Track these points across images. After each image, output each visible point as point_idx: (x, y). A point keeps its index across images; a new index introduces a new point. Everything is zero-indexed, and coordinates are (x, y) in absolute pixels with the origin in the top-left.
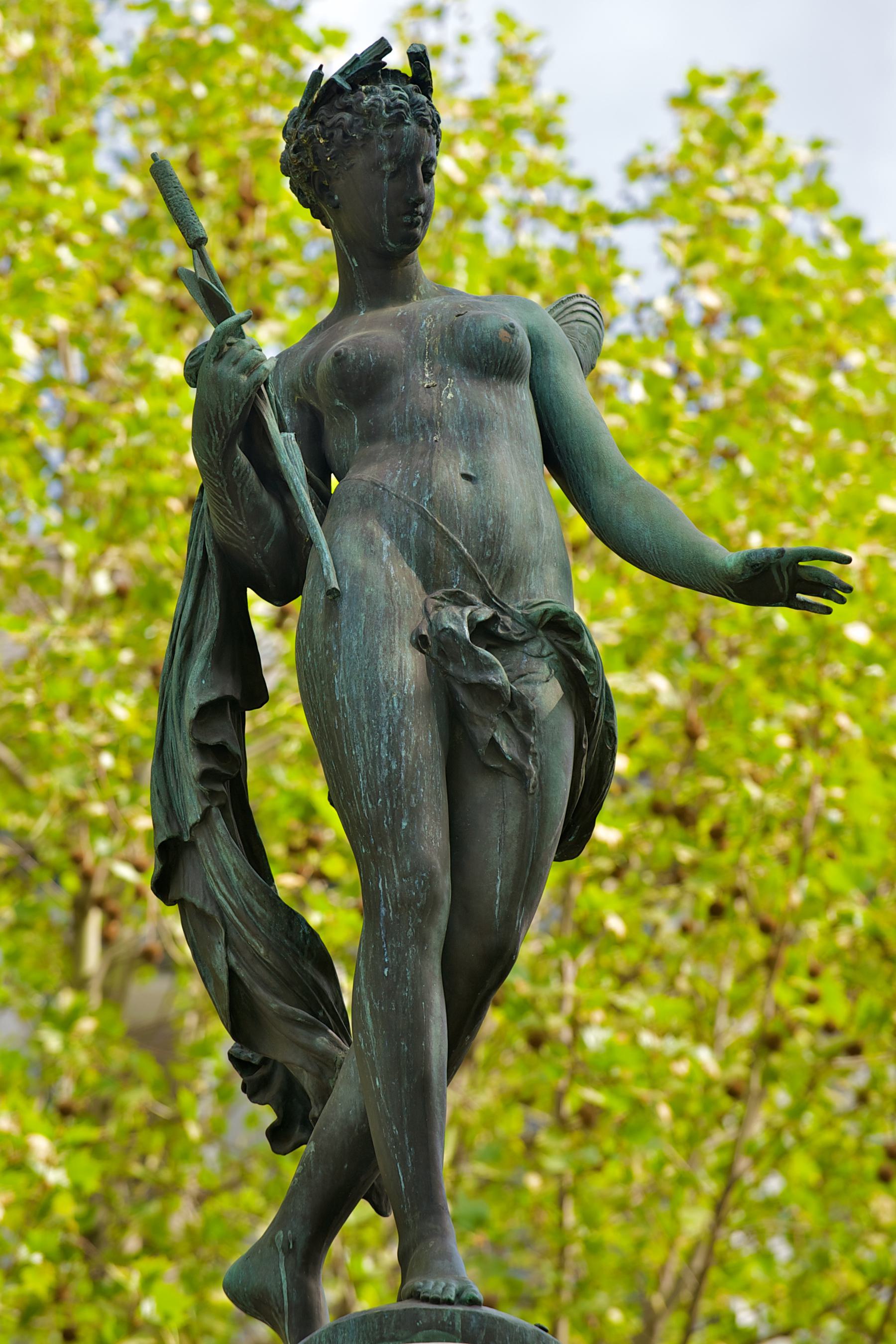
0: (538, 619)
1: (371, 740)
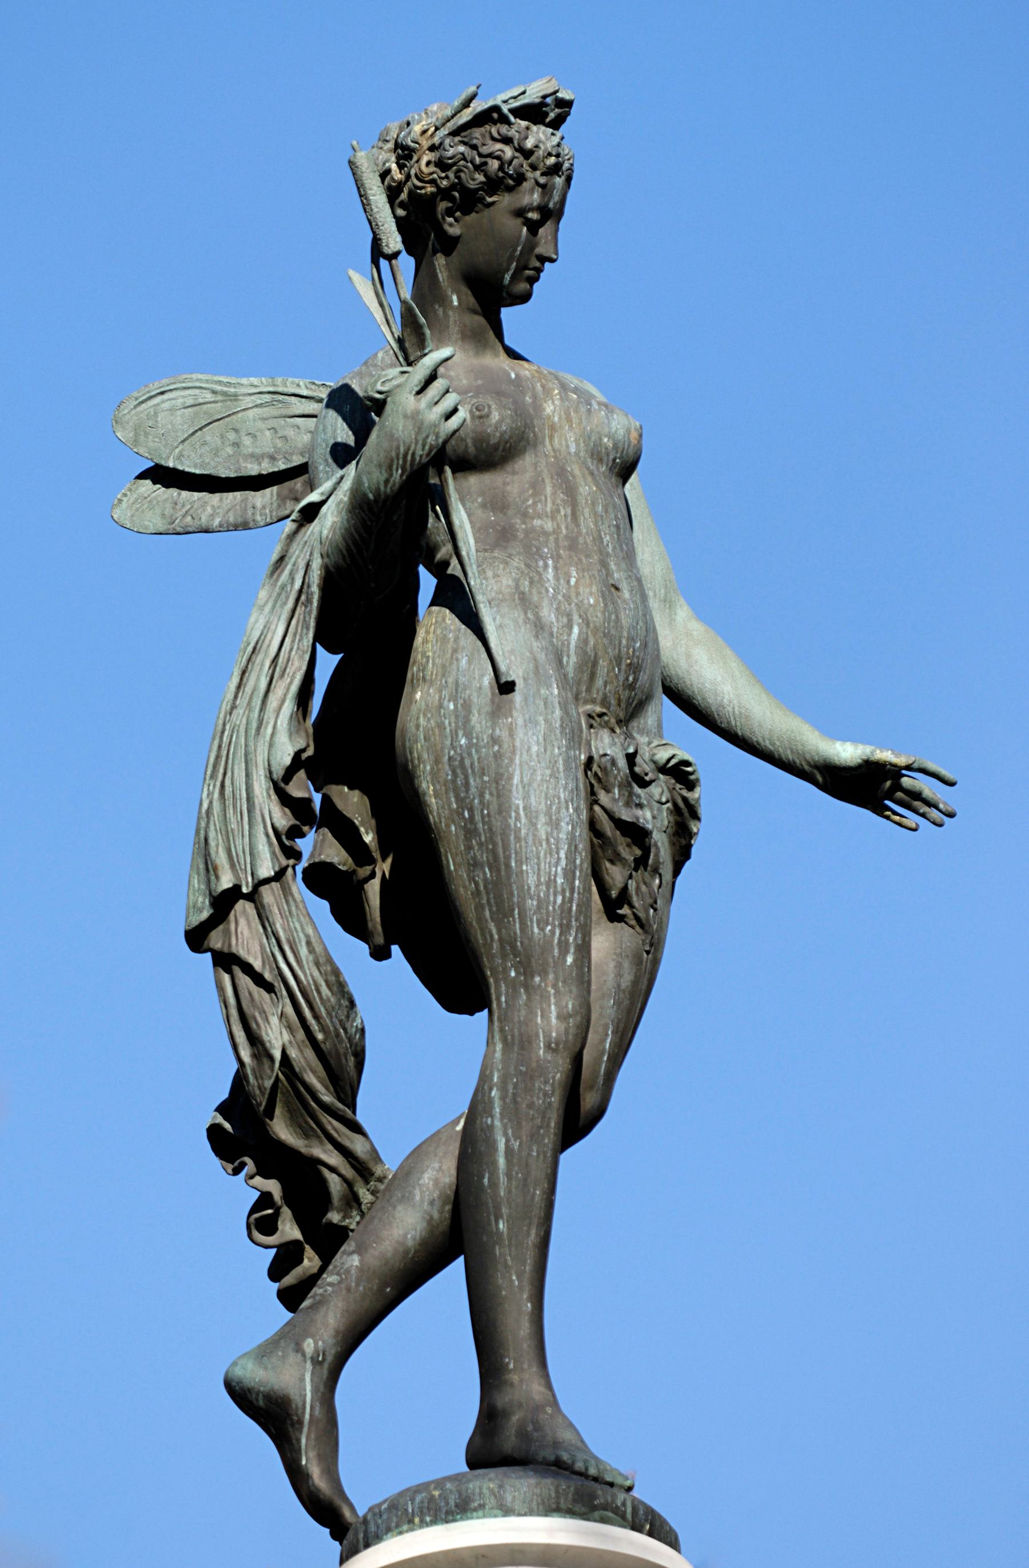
0: (664, 761)
1: (548, 860)
